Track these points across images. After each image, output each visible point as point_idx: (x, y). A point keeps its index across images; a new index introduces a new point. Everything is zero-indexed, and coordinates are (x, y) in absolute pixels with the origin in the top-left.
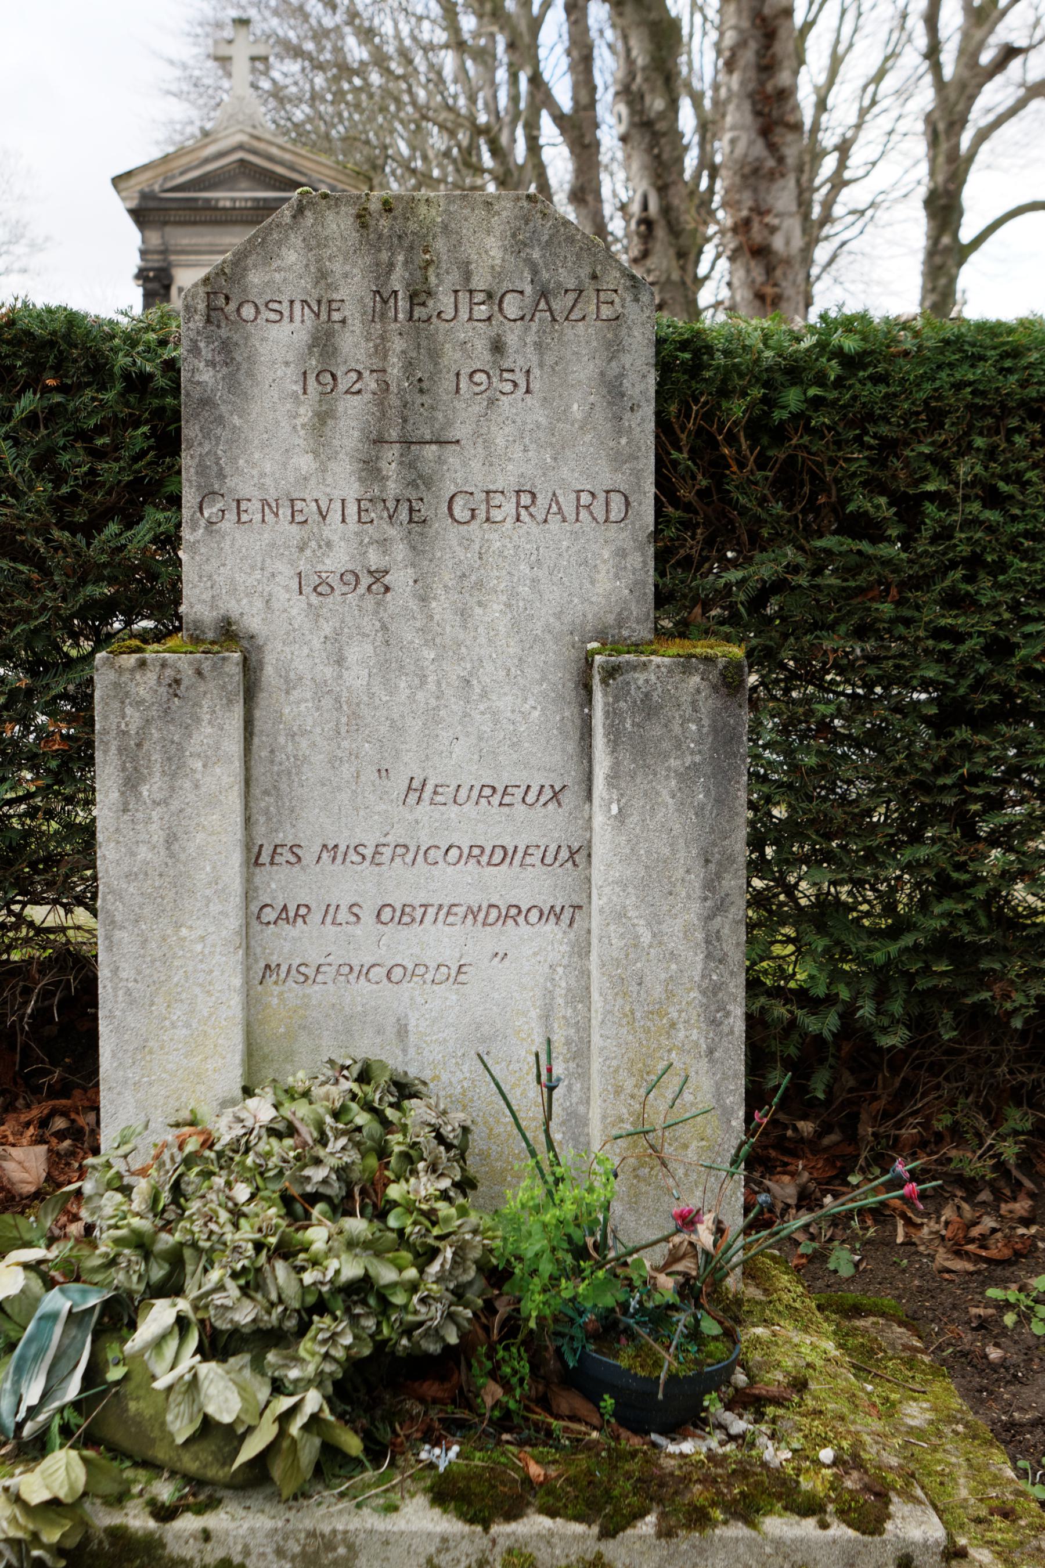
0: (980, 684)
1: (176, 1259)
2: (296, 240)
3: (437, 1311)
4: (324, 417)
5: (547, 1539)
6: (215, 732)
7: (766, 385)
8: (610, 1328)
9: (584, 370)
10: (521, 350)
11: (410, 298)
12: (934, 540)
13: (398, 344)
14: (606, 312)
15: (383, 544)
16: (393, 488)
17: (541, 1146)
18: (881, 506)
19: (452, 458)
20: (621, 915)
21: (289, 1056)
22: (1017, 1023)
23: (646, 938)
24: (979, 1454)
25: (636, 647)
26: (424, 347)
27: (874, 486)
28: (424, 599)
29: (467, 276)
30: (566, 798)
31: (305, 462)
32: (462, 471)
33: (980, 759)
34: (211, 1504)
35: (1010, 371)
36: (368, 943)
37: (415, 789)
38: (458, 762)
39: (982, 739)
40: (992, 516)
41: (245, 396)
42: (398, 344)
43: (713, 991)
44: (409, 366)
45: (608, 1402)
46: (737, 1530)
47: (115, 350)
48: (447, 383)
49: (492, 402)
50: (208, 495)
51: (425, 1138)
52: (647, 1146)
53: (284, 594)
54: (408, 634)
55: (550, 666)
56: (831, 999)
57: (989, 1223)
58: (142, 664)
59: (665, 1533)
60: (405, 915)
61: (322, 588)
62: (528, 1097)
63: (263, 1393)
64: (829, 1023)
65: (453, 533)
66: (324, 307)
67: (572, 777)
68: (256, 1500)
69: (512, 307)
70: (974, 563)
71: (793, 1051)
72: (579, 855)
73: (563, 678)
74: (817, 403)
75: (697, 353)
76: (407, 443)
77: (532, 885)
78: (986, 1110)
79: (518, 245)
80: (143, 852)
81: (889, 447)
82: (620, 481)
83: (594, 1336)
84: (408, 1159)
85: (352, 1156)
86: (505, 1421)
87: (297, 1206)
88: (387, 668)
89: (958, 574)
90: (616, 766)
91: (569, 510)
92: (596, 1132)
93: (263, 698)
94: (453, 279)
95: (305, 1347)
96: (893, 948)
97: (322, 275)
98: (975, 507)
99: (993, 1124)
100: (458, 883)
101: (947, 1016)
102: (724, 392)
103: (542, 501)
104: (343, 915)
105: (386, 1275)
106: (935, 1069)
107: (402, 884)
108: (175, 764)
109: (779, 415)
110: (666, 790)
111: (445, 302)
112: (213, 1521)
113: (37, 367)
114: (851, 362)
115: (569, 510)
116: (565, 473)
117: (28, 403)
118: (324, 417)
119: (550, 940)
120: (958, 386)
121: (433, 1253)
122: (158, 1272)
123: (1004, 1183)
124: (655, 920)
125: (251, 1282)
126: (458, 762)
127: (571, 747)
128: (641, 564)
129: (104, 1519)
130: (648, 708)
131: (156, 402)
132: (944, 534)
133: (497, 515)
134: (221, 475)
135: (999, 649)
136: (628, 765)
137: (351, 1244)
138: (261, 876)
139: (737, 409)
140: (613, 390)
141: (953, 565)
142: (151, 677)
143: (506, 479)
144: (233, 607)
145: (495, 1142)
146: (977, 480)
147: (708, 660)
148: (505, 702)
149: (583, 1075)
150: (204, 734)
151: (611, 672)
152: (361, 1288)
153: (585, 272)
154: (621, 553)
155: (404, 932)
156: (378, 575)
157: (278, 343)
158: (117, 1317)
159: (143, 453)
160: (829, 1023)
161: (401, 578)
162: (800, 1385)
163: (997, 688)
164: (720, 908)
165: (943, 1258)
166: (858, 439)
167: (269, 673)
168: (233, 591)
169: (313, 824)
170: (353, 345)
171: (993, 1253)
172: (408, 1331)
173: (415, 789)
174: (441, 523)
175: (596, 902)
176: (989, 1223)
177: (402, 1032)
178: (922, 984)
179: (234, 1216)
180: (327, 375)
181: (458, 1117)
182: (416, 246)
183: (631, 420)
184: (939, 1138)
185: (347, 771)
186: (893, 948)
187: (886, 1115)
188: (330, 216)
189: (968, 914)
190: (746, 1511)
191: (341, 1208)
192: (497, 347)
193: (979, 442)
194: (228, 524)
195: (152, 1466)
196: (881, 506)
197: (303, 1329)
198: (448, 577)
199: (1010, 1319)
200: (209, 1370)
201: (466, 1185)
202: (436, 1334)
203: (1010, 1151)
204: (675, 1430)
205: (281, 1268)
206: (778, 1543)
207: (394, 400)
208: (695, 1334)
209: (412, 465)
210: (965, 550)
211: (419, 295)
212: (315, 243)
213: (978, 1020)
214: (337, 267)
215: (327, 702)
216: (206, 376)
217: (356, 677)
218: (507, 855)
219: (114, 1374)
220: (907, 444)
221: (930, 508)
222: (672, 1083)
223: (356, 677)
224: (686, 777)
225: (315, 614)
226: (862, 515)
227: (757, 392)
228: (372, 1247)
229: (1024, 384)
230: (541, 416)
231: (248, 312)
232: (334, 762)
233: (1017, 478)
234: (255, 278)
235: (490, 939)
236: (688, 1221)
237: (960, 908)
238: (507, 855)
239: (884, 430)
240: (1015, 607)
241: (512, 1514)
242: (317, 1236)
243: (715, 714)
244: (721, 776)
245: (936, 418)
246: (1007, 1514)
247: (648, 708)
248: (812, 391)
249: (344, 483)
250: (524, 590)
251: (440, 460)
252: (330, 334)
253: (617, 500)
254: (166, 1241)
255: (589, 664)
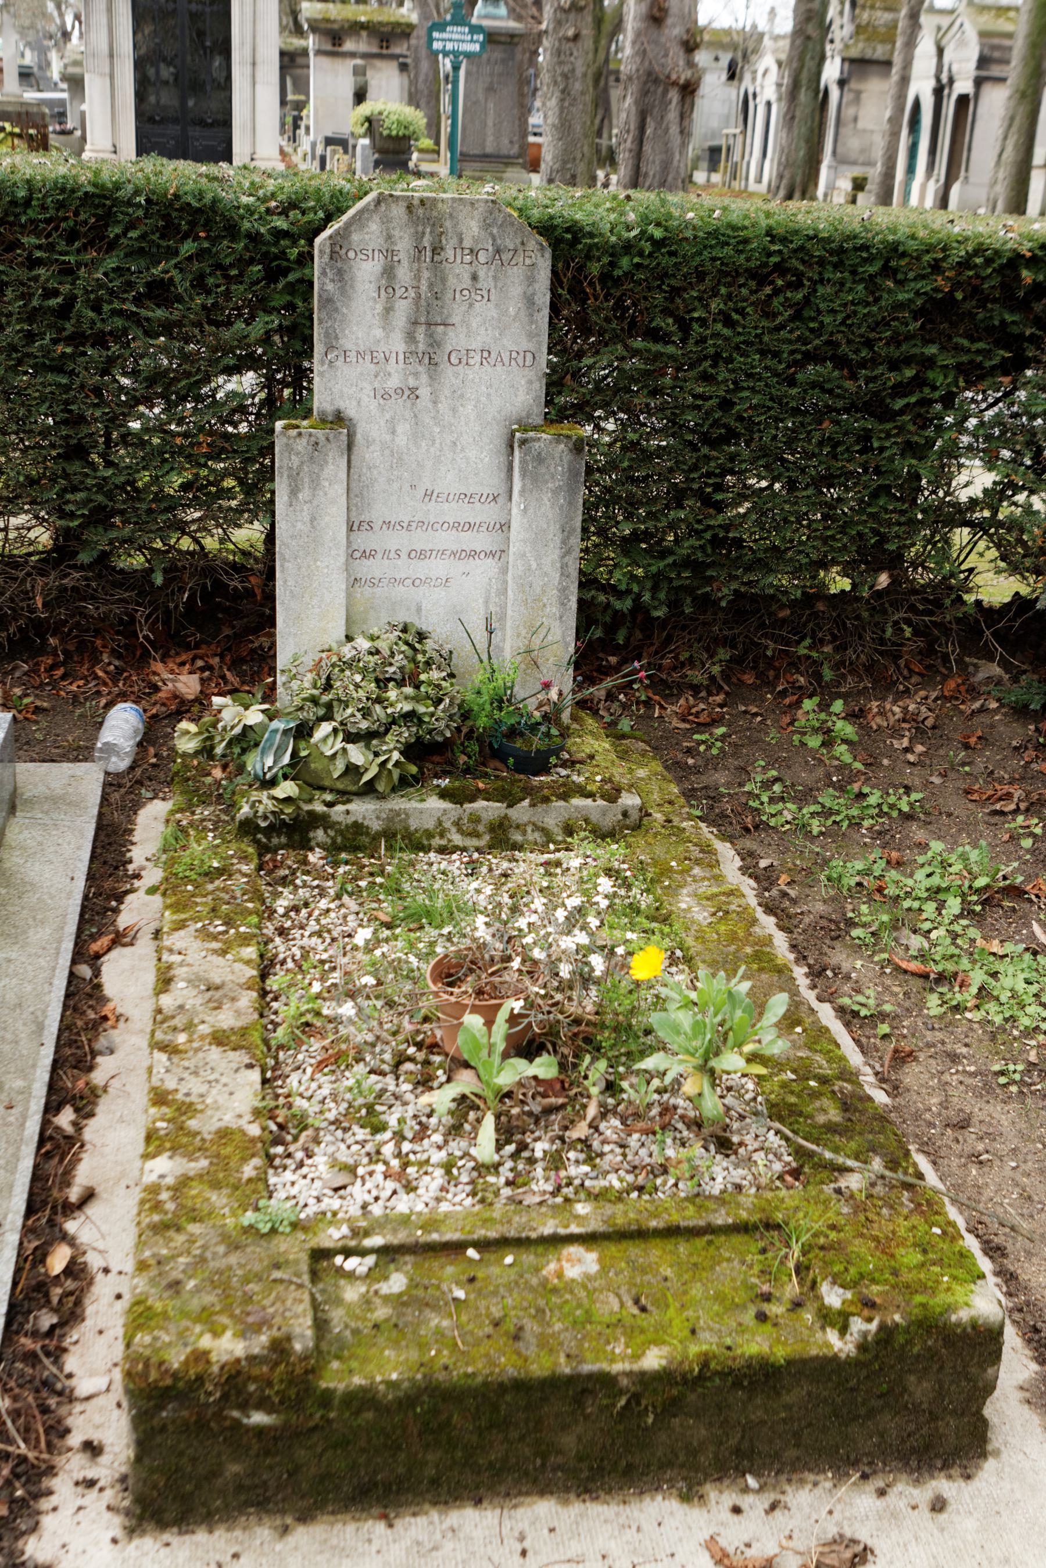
0: (716, 423)
1: (329, 706)
2: (376, 218)
3: (442, 724)
4: (388, 310)
5: (486, 809)
6: (335, 467)
7: (612, 255)
8: (513, 732)
9: (516, 290)
10: (486, 281)
11: (432, 252)
12: (697, 343)
13: (426, 274)
14: (528, 261)
15: (416, 375)
16: (421, 347)
17: (485, 657)
18: (669, 324)
19: (451, 332)
20: (523, 555)
21: (365, 621)
22: (724, 604)
23: (534, 566)
24: (665, 785)
25: (535, 428)
26: (439, 276)
27: (666, 312)
28: (435, 402)
29: (461, 241)
30: (500, 500)
31: (378, 333)
32: (455, 339)
33: (713, 464)
34: (349, 801)
35: (741, 252)
36: (405, 568)
37: (428, 495)
38: (449, 482)
39: (714, 453)
40: (726, 332)
41: (349, 298)
42: (426, 274)
43: (563, 590)
44: (431, 285)
45: (511, 760)
46: (561, 803)
47: (242, 218)
48: (449, 295)
49: (471, 305)
50: (330, 348)
51: (435, 655)
52: (530, 658)
53: (367, 398)
54: (427, 420)
55: (494, 437)
56: (629, 591)
57: (702, 706)
58: (300, 434)
59: (533, 805)
60: (422, 555)
61: (385, 396)
62: (480, 637)
63: (371, 757)
64: (625, 605)
65: (450, 370)
66: (390, 253)
67: (502, 489)
68: (367, 799)
69: (482, 257)
70: (716, 358)
71: (608, 619)
72: (505, 527)
73: (500, 443)
74: (638, 266)
75: (575, 235)
76: (429, 324)
77: (481, 541)
78: (707, 649)
79: (486, 226)
80: (299, 525)
81: (676, 291)
82: (531, 346)
83: (505, 736)
84: (428, 664)
85: (405, 662)
86: (467, 771)
87: (382, 683)
88: (416, 436)
89: (707, 364)
90: (524, 486)
91: (506, 360)
92: (508, 653)
93: (355, 450)
94: (454, 241)
95: (389, 738)
96: (662, 564)
97: (389, 237)
98: (719, 326)
99: (711, 657)
100: (447, 540)
101: (689, 600)
102: (588, 257)
103: (493, 355)
104: (392, 555)
105: (421, 709)
106: (684, 628)
107: (420, 540)
108: (315, 483)
109: (618, 273)
110: (546, 497)
111: (449, 253)
112: (349, 807)
113: (193, 224)
114: (658, 244)
115: (506, 360)
116: (505, 341)
117: (188, 248)
118: (388, 310)
119: (490, 566)
120: (714, 259)
121: (440, 701)
122: (321, 712)
123: (713, 685)
124: (538, 558)
125: (366, 713)
126: (449, 482)
127: (503, 475)
128: (539, 388)
129: (306, 807)
130: (540, 459)
131: (264, 249)
132: (703, 340)
133: (471, 362)
134: (337, 338)
135: (726, 404)
136: (529, 486)
137: (406, 698)
138: (353, 535)
139: (594, 269)
140: (530, 301)
141: (706, 358)
142: (304, 441)
143: (476, 344)
144: (342, 405)
145: (464, 658)
146: (721, 312)
147: (568, 437)
148: (472, 454)
149: (503, 629)
150: (329, 470)
151: (523, 442)
152: (410, 716)
153: (518, 241)
154: (530, 382)
155: (421, 563)
156: (413, 390)
157: (366, 271)
158: (303, 731)
159: (258, 282)
160: (627, 604)
161: (424, 392)
162: (592, 757)
163: (725, 426)
164: (568, 552)
165: (676, 723)
166: (659, 287)
167: (359, 437)
168: (342, 397)
169: (378, 511)
170: (404, 274)
171: (701, 720)
172: (430, 732)
173: (428, 495)
174: (444, 365)
175: (512, 549)
176: (702, 706)
177: (419, 609)
178: (675, 584)
179: (355, 687)
180: (390, 287)
181: (448, 647)
182: (435, 223)
183: (538, 316)
184: (683, 665)
185: (395, 486)
186: (662, 564)
187: (656, 653)
188: (393, 206)
189: (702, 547)
190: (565, 797)
191: (401, 684)
192: (475, 278)
193: (723, 290)
194: (340, 363)
195: (322, 789)
196: (669, 324)
197: (387, 731)
198: (447, 392)
199: (702, 748)
200: (349, 746)
201: (452, 675)
202: (442, 733)
203: (716, 670)
204: (536, 774)
205: (378, 707)
206: (576, 807)
207: (423, 303)
208: (548, 735)
209: (431, 336)
210: (711, 351)
211: (437, 249)
212: (386, 221)
213: (706, 603)
214: (396, 233)
215: (387, 452)
216: (330, 287)
217: (401, 440)
218: (471, 526)
219: (303, 754)
220: (685, 290)
221: (695, 326)
222: (543, 632)
223: (401, 440)
224: (555, 492)
225: (382, 408)
226: (658, 329)
227: (606, 260)
228: (416, 699)
229: (748, 260)
230: (494, 313)
231: (351, 254)
232: (389, 481)
233: (742, 312)
234: (355, 237)
235: (462, 566)
236: (547, 686)
237: (697, 543)
238: (471, 526)
239: (673, 282)
240: (735, 383)
241: (472, 800)
242: (392, 694)
243: (570, 462)
244: (572, 491)
245: (701, 276)
246: (670, 802)
247: (540, 459)
248: (636, 260)
249: (398, 344)
250: (483, 399)
251: (445, 334)
252: (392, 268)
253: (529, 356)
254: (325, 698)
255: (513, 436)
